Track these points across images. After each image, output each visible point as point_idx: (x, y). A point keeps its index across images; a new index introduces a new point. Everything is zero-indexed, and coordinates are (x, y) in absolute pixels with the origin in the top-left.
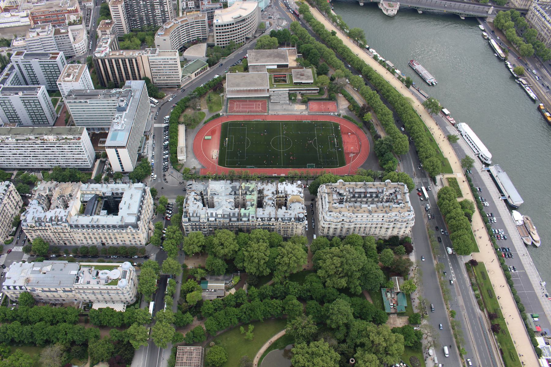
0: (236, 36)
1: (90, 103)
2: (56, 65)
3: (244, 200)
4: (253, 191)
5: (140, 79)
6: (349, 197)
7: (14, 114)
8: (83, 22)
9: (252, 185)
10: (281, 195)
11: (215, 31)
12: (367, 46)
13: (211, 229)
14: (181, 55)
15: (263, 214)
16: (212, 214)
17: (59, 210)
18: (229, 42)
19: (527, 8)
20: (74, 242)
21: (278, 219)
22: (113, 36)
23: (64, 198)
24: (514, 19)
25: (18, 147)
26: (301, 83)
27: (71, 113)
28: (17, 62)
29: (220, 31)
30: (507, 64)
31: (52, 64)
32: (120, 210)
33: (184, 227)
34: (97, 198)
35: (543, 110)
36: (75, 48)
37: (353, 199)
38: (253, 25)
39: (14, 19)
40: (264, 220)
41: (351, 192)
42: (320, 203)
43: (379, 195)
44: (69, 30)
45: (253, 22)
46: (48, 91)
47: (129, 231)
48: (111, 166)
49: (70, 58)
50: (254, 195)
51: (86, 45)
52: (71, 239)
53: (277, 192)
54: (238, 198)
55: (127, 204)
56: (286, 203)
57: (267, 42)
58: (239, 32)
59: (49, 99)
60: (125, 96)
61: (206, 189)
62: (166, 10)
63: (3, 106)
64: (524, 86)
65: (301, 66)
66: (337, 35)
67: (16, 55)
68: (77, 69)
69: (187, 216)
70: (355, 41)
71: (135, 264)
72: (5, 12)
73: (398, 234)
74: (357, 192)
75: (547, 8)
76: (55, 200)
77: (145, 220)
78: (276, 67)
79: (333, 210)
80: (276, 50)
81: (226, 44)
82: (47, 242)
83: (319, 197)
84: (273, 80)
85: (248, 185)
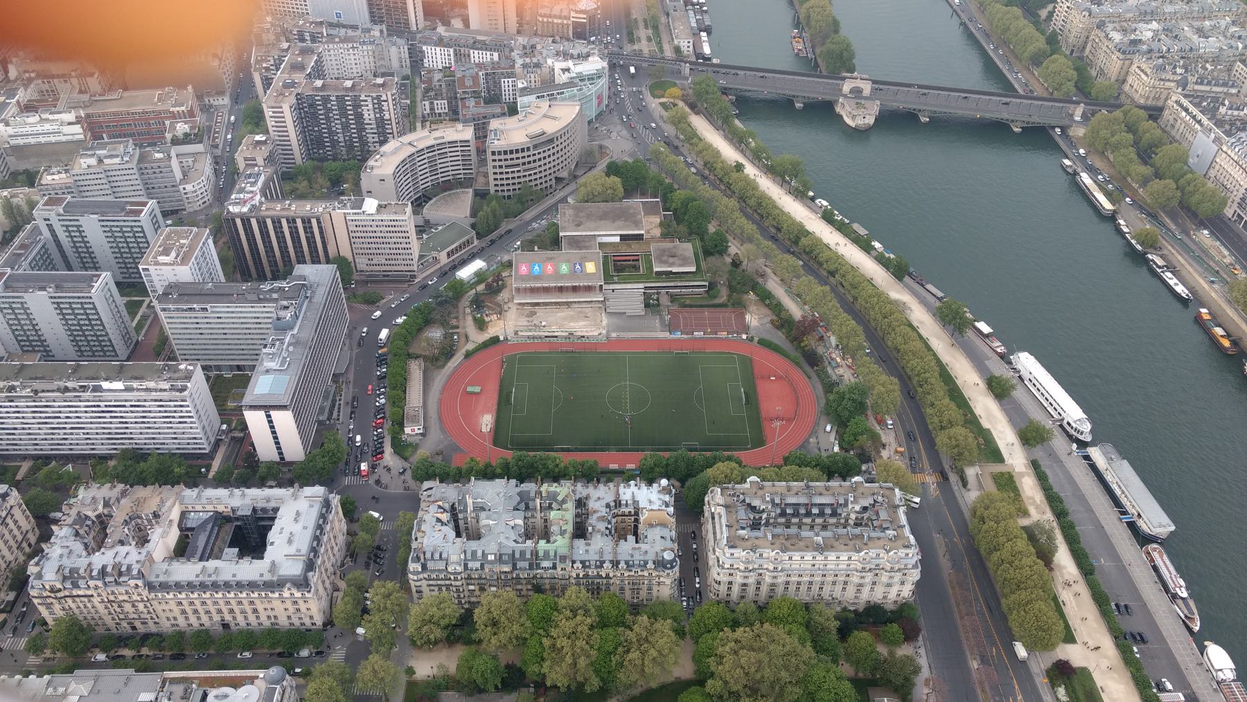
0: (535, 174)
1: (213, 312)
2: (91, 306)
3: (546, 521)
4: (564, 501)
5: (328, 262)
6: (773, 514)
7: (34, 333)
8: (206, 138)
9: (563, 489)
10: (627, 510)
11: (490, 164)
12: (811, 194)
13: (472, 587)
14: (415, 213)
15: (587, 551)
16: (474, 553)
17: (123, 550)
18: (520, 186)
19: (1160, 104)
20: (155, 623)
21: (618, 563)
22: (270, 170)
23: (139, 521)
24: (1131, 128)
25: (36, 407)
26: (671, 273)
27: (169, 332)
28: (49, 220)
29: (501, 163)
30: (1119, 224)
31: (132, 227)
32: (269, 548)
33: (412, 583)
34: (220, 519)
35: (1207, 323)
36: (186, 194)
37: (782, 520)
38: (571, 152)
39: (47, 127)
40: (589, 567)
41: (777, 505)
42: (710, 527)
43: (839, 511)
44: (173, 154)
45: (571, 146)
46: (118, 284)
47: (286, 594)
48: (254, 449)
49: (174, 214)
50: (565, 510)
51: (209, 187)
52: (148, 616)
53: (618, 503)
54: (533, 516)
55: (286, 535)
56: (636, 527)
57: (599, 189)
58: (540, 166)
59: (121, 301)
60: (292, 299)
61: (464, 497)
62: (387, 117)
63: (8, 317)
64: (1159, 270)
65: (667, 235)
66: (746, 171)
67: (46, 204)
68: (187, 238)
69: (418, 559)
70: (783, 183)
71: (298, 670)
72: (27, 112)
73: (885, 598)
74: (790, 504)
76: (115, 527)
77: (326, 570)
78: (617, 239)
79: (738, 543)
80: (617, 205)
81: (514, 190)
82: (89, 625)
83: (706, 514)
84: (611, 268)
85: (554, 487)
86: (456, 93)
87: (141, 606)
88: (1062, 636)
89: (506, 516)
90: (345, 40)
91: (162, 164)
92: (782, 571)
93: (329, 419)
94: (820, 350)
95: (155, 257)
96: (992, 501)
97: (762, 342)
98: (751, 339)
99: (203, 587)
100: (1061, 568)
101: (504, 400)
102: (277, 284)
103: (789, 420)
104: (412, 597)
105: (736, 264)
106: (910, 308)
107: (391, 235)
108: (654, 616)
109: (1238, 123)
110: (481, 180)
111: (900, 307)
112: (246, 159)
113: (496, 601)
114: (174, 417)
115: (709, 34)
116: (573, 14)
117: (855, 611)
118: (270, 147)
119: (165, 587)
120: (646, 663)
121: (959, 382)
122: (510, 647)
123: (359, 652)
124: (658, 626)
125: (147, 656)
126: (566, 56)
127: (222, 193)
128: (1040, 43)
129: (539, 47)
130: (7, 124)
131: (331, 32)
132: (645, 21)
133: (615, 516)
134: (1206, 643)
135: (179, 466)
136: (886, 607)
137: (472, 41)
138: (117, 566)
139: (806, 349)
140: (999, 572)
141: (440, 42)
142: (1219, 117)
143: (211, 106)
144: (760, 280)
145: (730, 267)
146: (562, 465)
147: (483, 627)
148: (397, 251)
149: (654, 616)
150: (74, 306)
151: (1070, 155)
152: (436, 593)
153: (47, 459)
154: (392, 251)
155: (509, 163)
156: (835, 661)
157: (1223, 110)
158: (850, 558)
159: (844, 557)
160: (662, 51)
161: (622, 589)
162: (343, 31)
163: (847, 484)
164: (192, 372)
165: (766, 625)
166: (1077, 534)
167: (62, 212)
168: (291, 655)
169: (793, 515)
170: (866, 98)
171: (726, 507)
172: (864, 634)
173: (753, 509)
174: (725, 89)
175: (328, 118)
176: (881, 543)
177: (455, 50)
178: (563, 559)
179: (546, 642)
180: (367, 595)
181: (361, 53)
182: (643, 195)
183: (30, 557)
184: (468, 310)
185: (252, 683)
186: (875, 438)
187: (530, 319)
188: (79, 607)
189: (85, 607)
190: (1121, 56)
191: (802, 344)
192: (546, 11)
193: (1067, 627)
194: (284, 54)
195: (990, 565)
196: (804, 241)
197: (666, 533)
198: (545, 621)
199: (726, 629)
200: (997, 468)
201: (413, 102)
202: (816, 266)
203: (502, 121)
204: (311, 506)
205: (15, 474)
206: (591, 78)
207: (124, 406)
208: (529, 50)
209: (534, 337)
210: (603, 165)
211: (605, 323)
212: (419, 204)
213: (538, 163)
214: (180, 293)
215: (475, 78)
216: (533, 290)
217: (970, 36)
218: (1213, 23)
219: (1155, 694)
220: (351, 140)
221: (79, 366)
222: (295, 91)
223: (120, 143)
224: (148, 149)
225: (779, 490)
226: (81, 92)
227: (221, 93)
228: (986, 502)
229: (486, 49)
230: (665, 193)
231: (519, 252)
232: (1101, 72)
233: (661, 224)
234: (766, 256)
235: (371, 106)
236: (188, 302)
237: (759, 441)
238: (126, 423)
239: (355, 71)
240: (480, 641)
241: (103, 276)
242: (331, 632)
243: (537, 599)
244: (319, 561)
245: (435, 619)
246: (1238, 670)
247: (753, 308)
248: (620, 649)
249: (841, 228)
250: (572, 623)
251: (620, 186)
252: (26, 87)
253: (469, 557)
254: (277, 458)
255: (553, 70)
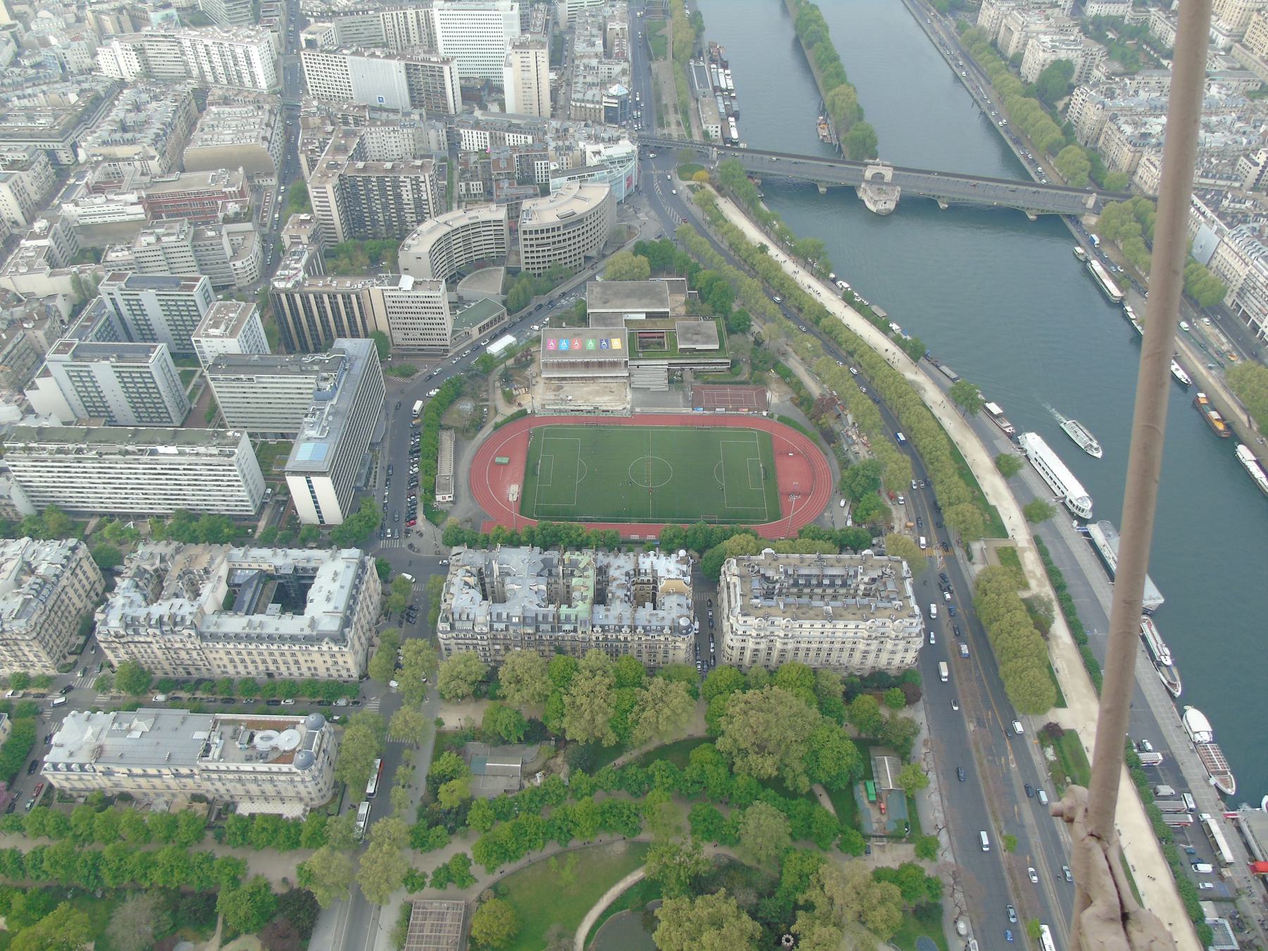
1: (258, 382)
2: (148, 375)
3: (568, 586)
4: (585, 569)
5: (366, 336)
6: (786, 584)
8: (255, 217)
9: (584, 558)
10: (646, 579)
11: (522, 243)
12: (832, 276)
13: (497, 647)
14: (449, 289)
15: (607, 616)
16: (499, 615)
17: (178, 602)
18: (550, 264)
22: (313, 248)
23: (192, 576)
26: (695, 350)
29: (532, 242)
32: (309, 605)
34: (265, 577)
37: (795, 590)
40: (608, 631)
42: (725, 596)
43: (849, 582)
44: (224, 232)
45: (600, 226)
46: (173, 355)
47: (325, 648)
49: (223, 289)
50: (587, 577)
52: (201, 663)
53: (637, 572)
55: (324, 594)
56: (654, 595)
57: (626, 267)
59: (176, 370)
60: (332, 371)
61: (490, 562)
62: (425, 197)
63: (77, 384)
66: (769, 253)
68: (236, 311)
69: (447, 619)
70: (806, 265)
71: (336, 718)
74: (802, 575)
75: (1209, 196)
77: (362, 627)
78: (643, 317)
80: (644, 283)
83: (723, 583)
85: (576, 556)
86: (491, 175)
87: (194, 654)
88: (1054, 701)
89: (531, 582)
90: (387, 123)
91: (214, 242)
92: (793, 637)
93: (366, 485)
94: (837, 428)
95: (206, 330)
96: (994, 575)
97: (781, 419)
98: (770, 416)
99: (249, 638)
100: (1056, 637)
101: (530, 472)
102: (318, 357)
103: (806, 495)
104: (441, 654)
105: (758, 343)
106: (924, 389)
107: (426, 310)
108: (669, 678)
109: (1240, 216)
110: (513, 258)
111: (914, 388)
112: (291, 237)
113: (520, 660)
114: (222, 481)
115: (737, 119)
116: (605, 99)
117: (861, 677)
118: (314, 226)
119: (215, 637)
120: (660, 720)
121: (968, 461)
122: (533, 703)
123: (392, 703)
124: (672, 687)
125: (201, 699)
126: (598, 139)
127: (269, 267)
128: (1057, 134)
129: (571, 130)
130: (77, 205)
131: (373, 115)
132: (675, 106)
133: (634, 584)
134: (1186, 707)
135: (228, 527)
136: (890, 672)
137: (507, 125)
138: (172, 617)
139: (824, 426)
140: (998, 642)
141: (477, 125)
142: (1222, 209)
143: (260, 187)
144: (781, 359)
145: (752, 346)
146: (585, 535)
147: (507, 684)
148: (431, 326)
149: (669, 678)
150: (134, 375)
151: (1082, 242)
152: (464, 651)
153: (112, 516)
154: (427, 326)
155: (540, 242)
156: (839, 723)
157: (1225, 203)
158: (857, 627)
159: (852, 625)
160: (690, 135)
161: (639, 651)
162: (385, 115)
163: (858, 556)
164: (239, 438)
165: (775, 688)
166: (1073, 606)
167: (123, 286)
168: (330, 703)
169: (805, 586)
170: (887, 184)
171: (741, 576)
172: (868, 697)
173: (767, 579)
174: (752, 173)
175: (369, 199)
176: (887, 612)
177: (491, 134)
178: (584, 623)
179: (566, 699)
180: (400, 651)
181: (401, 136)
182: (670, 274)
183: (98, 605)
184: (497, 384)
185: (294, 728)
186: (887, 513)
187: (557, 393)
188: (140, 652)
189: (146, 652)
190: (1132, 149)
191: (820, 422)
192: (579, 96)
193: (1059, 692)
194: (329, 136)
195: (990, 635)
196: (824, 321)
197: (683, 601)
198: (565, 680)
199: (736, 691)
200: (1001, 543)
201: (451, 183)
202: (835, 346)
203: (534, 202)
204: (348, 567)
205: (84, 530)
206: (622, 161)
207: (178, 469)
208: (562, 134)
209: (560, 411)
210: (630, 245)
211: (629, 397)
212: (452, 281)
213: (568, 243)
214: (228, 363)
215: (510, 160)
216: (560, 366)
217: (991, 127)
218: (1219, 118)
219: (1135, 754)
220: (390, 220)
221: (137, 431)
222: (338, 172)
223: (176, 221)
224: (202, 227)
225: (793, 562)
226: (143, 174)
227: (270, 174)
228: (989, 576)
229: (521, 133)
230: (690, 272)
231: (548, 328)
232: (1113, 163)
233: (686, 303)
234: (788, 335)
235: (409, 187)
236: (235, 372)
237: (776, 516)
238: (180, 485)
239: (395, 153)
240: (504, 697)
241: (159, 347)
242: (366, 684)
243: (559, 660)
244: (355, 619)
245: (462, 675)
246: (1215, 733)
247: (774, 386)
248: (636, 708)
249: (861, 309)
250: (591, 683)
251: (646, 264)
252: (94, 169)
253: (494, 618)
254: (318, 522)
255: (585, 153)
